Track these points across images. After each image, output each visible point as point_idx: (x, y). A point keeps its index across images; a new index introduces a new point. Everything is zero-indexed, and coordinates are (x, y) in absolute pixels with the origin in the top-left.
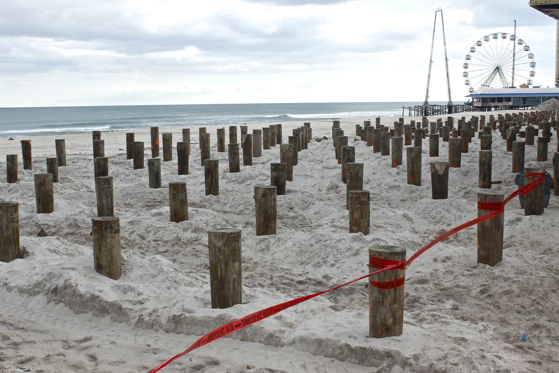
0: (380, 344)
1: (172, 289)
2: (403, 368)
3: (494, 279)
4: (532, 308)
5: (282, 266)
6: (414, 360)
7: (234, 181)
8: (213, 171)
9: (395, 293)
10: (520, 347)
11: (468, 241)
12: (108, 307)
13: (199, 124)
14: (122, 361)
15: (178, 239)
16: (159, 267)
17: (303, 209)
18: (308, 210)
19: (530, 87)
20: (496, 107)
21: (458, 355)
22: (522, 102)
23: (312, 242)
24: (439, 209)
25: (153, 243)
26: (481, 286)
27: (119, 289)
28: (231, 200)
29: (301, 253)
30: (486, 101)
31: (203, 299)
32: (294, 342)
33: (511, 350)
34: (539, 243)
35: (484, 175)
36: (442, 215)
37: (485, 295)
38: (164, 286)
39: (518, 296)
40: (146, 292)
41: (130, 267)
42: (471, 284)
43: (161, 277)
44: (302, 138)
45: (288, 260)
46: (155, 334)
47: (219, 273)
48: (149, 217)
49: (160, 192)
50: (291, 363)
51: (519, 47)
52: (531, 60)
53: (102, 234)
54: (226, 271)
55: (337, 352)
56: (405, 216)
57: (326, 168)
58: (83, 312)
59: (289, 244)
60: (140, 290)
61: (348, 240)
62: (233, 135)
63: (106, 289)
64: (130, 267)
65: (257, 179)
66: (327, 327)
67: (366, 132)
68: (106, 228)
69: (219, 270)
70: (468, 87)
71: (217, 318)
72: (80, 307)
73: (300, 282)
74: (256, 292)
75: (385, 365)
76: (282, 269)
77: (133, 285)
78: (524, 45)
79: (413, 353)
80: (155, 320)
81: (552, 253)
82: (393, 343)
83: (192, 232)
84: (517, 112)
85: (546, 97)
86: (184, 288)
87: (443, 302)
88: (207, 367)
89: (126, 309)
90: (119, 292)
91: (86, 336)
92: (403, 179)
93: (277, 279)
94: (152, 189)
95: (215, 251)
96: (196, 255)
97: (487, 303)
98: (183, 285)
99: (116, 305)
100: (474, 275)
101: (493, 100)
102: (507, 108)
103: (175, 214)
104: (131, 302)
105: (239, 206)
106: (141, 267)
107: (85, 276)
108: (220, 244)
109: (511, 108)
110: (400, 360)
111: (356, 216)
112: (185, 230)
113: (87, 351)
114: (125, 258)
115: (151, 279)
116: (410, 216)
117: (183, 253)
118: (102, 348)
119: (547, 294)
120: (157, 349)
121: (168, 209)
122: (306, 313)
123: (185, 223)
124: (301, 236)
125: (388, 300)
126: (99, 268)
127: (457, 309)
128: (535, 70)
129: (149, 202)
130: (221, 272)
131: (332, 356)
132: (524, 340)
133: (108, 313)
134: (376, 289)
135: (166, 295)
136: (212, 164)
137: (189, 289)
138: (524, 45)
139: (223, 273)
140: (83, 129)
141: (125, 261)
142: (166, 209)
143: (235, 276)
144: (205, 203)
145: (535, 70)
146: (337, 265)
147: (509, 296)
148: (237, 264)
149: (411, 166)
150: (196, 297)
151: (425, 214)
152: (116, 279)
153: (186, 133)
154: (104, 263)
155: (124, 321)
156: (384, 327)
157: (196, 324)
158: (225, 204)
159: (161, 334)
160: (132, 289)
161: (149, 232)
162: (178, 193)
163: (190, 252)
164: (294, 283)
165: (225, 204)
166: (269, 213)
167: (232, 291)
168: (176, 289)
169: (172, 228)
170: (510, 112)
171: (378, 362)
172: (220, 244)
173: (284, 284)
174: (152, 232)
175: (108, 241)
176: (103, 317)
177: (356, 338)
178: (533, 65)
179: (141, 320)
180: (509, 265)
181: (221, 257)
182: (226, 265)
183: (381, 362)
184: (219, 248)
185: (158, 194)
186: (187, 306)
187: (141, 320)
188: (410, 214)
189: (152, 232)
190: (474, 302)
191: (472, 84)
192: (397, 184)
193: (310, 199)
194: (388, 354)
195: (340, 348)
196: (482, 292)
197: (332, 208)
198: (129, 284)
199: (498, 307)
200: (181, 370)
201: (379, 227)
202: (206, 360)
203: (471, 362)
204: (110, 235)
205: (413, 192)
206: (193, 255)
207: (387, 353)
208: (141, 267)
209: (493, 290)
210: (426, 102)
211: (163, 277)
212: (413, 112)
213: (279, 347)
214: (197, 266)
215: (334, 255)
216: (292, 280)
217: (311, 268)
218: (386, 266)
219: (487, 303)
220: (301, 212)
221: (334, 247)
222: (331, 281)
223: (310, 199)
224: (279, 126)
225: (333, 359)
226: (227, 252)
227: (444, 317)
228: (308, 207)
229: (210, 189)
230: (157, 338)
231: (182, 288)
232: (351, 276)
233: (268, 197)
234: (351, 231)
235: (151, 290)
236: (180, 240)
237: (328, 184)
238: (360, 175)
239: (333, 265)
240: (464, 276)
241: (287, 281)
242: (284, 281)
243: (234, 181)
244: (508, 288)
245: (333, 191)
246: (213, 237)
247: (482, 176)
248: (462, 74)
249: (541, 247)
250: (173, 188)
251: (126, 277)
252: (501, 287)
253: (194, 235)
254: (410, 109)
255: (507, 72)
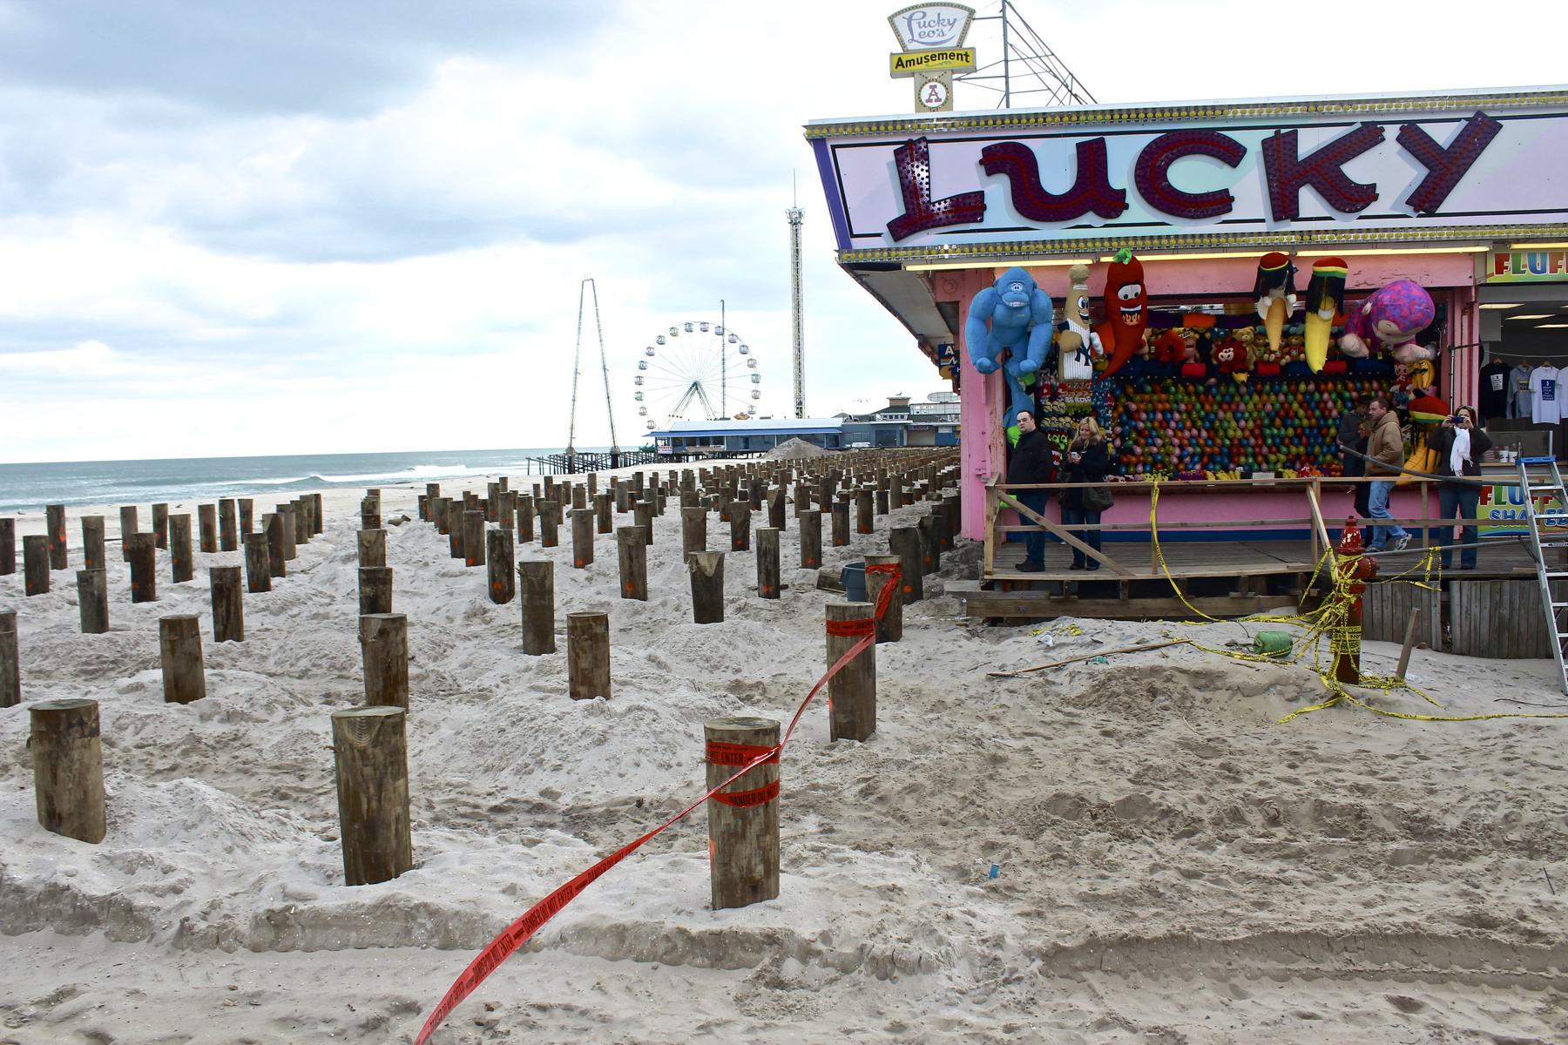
0: (747, 919)
1: (238, 851)
2: (804, 961)
3: (878, 765)
4: (965, 813)
5: (449, 779)
6: (824, 942)
7: (263, 610)
8: (229, 590)
9: (766, 813)
10: (994, 889)
11: (788, 699)
12: (96, 909)
13: (119, 500)
14: (181, 1033)
15: (195, 740)
16: (198, 805)
17: (436, 659)
18: (446, 661)
19: (756, 417)
20: (697, 455)
21: (900, 921)
22: (742, 445)
23: (503, 724)
24: (715, 642)
25: (135, 752)
26: (859, 781)
27: (112, 863)
28: (274, 649)
29: (480, 748)
30: (681, 444)
31: (321, 867)
32: (563, 939)
33: (983, 897)
34: (919, 693)
35: (768, 573)
36: (722, 652)
37: (872, 798)
38: (218, 845)
39: (933, 794)
40: (181, 866)
41: (124, 811)
42: (838, 780)
43: (206, 828)
44: (305, 517)
45: (454, 765)
46: (226, 959)
47: (365, 807)
48: (114, 695)
49: (110, 641)
50: (568, 984)
51: (733, 349)
52: (752, 371)
53: (58, 742)
54: (379, 801)
55: (662, 947)
56: (651, 659)
57: (444, 575)
58: (27, 930)
59: (446, 731)
60: (168, 862)
61: (578, 714)
62: (227, 520)
63: (79, 866)
64: (124, 811)
65: (310, 603)
66: (620, 897)
67: (433, 506)
68: (70, 726)
69: (364, 800)
70: (645, 419)
71: (376, 907)
72: (17, 917)
73: (497, 810)
74: (432, 840)
75: (767, 961)
76: (448, 784)
77: (150, 851)
78: (739, 343)
79: (818, 930)
80: (224, 926)
81: (946, 708)
82: (769, 913)
83: (222, 721)
84: (733, 462)
85: (783, 436)
86: (263, 846)
87: (798, 821)
88: (393, 1020)
89: (143, 909)
90: (116, 871)
91: (59, 985)
92: (612, 590)
93: (444, 807)
94: (91, 636)
95: (354, 759)
96: (246, 772)
97: (879, 813)
98: (259, 839)
99: (117, 903)
100: (841, 761)
101: (692, 441)
102: (715, 456)
103: (176, 686)
104: (152, 890)
105: (298, 659)
106: (153, 807)
107: (20, 841)
108: (364, 742)
109: (723, 455)
110: (795, 948)
111: (584, 664)
112: (204, 718)
113: (77, 1024)
114: (109, 791)
115: (183, 833)
116: (663, 659)
117: (214, 768)
118: (112, 1012)
119: (982, 785)
120: (258, 994)
121: (158, 674)
122: (558, 873)
123: (202, 704)
124: (465, 713)
125: (754, 829)
126: (53, 819)
127: (831, 831)
128: (760, 387)
129: (86, 663)
130: (369, 802)
131: (653, 957)
132: (993, 875)
133: (98, 923)
134: (728, 809)
135: (227, 866)
136: (229, 574)
137: (273, 846)
138: (739, 343)
139: (374, 804)
140: (32, 501)
141: (110, 798)
142: (154, 676)
143: (399, 809)
144: (220, 659)
145: (760, 387)
146: (567, 767)
147: (915, 795)
148: (401, 782)
149: (627, 562)
150: (303, 865)
151: (689, 654)
152: (95, 840)
153: (56, 515)
154: (65, 805)
155: (143, 937)
156: (742, 883)
157: (327, 925)
158: (264, 658)
159: (242, 956)
160: (147, 862)
161: (122, 728)
162: (182, 638)
163: (229, 765)
164: (483, 811)
165: (264, 658)
166: (394, 671)
167: (394, 842)
168: (245, 850)
169: (176, 716)
170: (722, 463)
171: (752, 956)
172: (364, 742)
173: (463, 816)
174: (131, 729)
175: (76, 755)
176: (85, 933)
177: (691, 914)
178: (756, 379)
179: (185, 930)
180: (891, 737)
181: (368, 771)
182: (380, 787)
183: (757, 956)
184: (363, 752)
185: (106, 645)
186: (294, 887)
187: (185, 930)
188: (661, 654)
189: (131, 729)
190: (855, 814)
191: (651, 415)
192: (603, 598)
193: (445, 638)
194: (771, 939)
195: (667, 938)
196: (865, 793)
197: (495, 654)
198: (137, 850)
199: (904, 819)
200: (337, 1034)
201: (624, 683)
202: (386, 1004)
203: (933, 931)
204: (78, 742)
205: (636, 613)
206: (239, 770)
207: (768, 936)
208: (153, 807)
209: (886, 787)
210: (571, 448)
211: (214, 827)
212: (546, 467)
213: (531, 953)
214: (255, 794)
215: (556, 748)
216: (476, 807)
217: (510, 778)
218: (751, 759)
219: (879, 813)
220: (431, 666)
221: (552, 730)
222: (560, 800)
223: (445, 638)
224: (317, 497)
225: (655, 964)
226: (381, 758)
227: (838, 850)
228: (443, 655)
229: (226, 628)
230: (235, 968)
231: (259, 846)
232: (598, 787)
233: (392, 637)
234: (575, 695)
235: (190, 858)
236: (199, 740)
237: (465, 607)
238: (547, 583)
239: (557, 768)
240: (820, 765)
241: (469, 810)
242: (462, 810)
243: (263, 610)
244: (911, 781)
245: (477, 620)
246: (346, 728)
247: (763, 577)
248: (633, 396)
249: (925, 700)
250: (171, 630)
251: (119, 834)
252: (896, 780)
253: (227, 728)
254: (541, 460)
255: (711, 388)
